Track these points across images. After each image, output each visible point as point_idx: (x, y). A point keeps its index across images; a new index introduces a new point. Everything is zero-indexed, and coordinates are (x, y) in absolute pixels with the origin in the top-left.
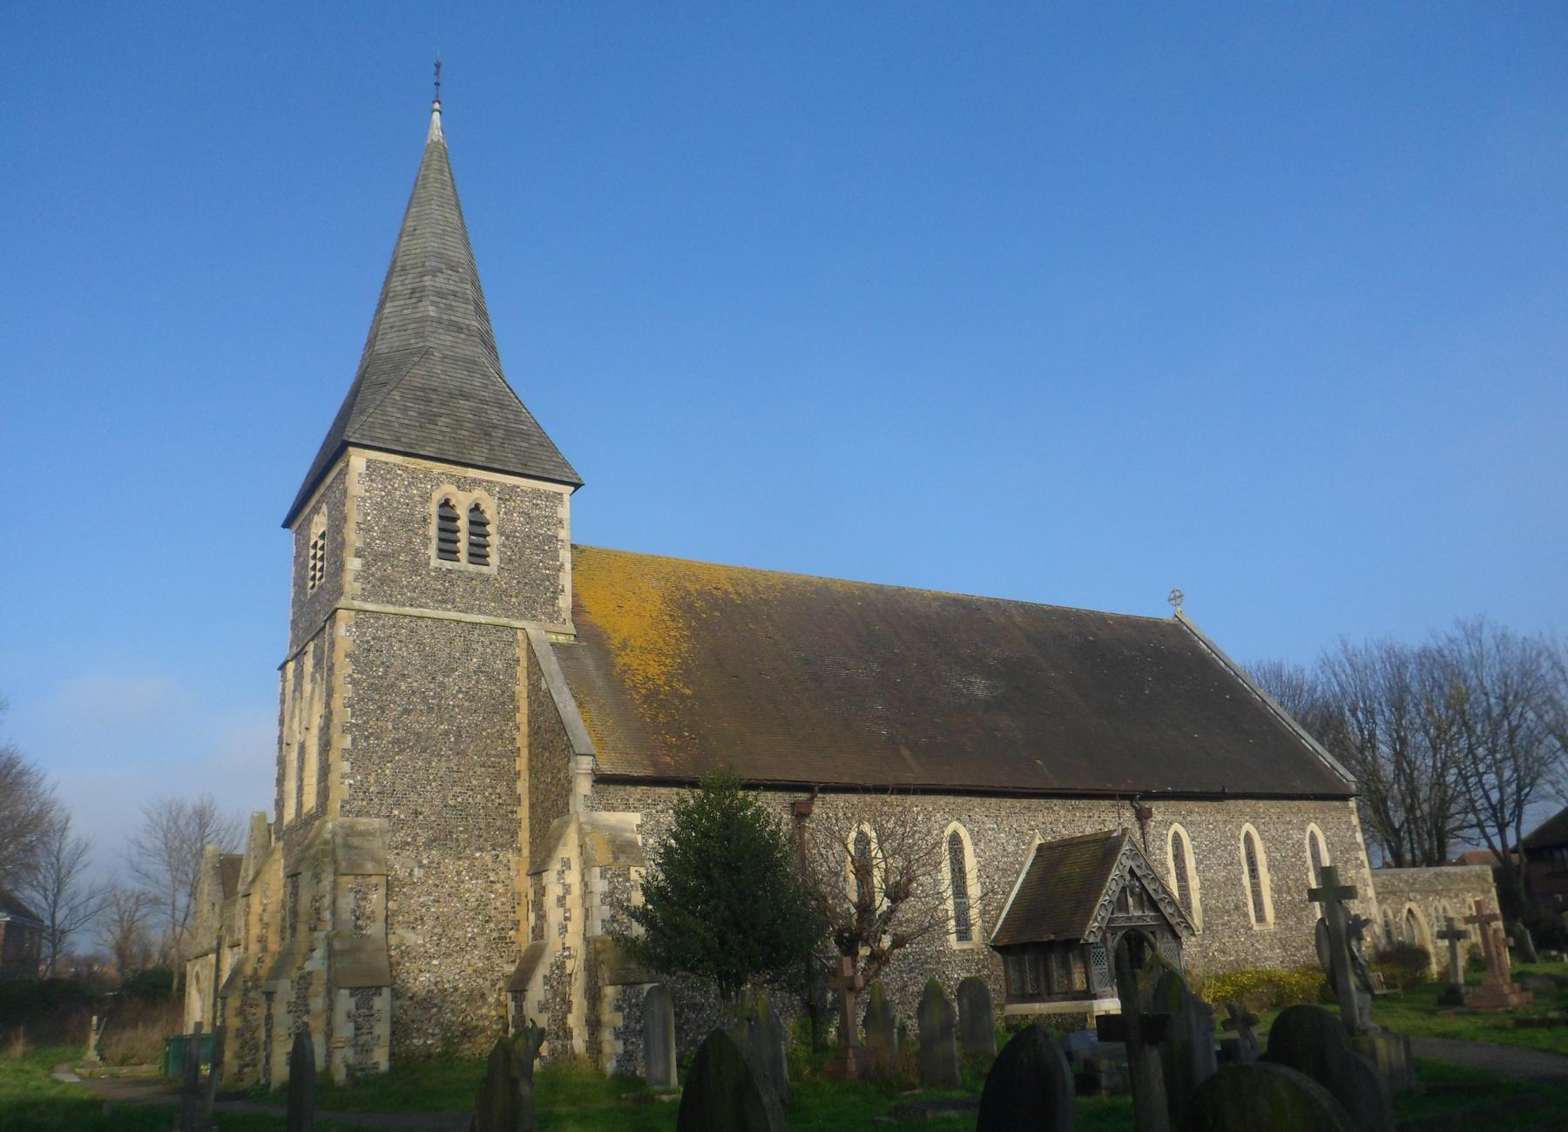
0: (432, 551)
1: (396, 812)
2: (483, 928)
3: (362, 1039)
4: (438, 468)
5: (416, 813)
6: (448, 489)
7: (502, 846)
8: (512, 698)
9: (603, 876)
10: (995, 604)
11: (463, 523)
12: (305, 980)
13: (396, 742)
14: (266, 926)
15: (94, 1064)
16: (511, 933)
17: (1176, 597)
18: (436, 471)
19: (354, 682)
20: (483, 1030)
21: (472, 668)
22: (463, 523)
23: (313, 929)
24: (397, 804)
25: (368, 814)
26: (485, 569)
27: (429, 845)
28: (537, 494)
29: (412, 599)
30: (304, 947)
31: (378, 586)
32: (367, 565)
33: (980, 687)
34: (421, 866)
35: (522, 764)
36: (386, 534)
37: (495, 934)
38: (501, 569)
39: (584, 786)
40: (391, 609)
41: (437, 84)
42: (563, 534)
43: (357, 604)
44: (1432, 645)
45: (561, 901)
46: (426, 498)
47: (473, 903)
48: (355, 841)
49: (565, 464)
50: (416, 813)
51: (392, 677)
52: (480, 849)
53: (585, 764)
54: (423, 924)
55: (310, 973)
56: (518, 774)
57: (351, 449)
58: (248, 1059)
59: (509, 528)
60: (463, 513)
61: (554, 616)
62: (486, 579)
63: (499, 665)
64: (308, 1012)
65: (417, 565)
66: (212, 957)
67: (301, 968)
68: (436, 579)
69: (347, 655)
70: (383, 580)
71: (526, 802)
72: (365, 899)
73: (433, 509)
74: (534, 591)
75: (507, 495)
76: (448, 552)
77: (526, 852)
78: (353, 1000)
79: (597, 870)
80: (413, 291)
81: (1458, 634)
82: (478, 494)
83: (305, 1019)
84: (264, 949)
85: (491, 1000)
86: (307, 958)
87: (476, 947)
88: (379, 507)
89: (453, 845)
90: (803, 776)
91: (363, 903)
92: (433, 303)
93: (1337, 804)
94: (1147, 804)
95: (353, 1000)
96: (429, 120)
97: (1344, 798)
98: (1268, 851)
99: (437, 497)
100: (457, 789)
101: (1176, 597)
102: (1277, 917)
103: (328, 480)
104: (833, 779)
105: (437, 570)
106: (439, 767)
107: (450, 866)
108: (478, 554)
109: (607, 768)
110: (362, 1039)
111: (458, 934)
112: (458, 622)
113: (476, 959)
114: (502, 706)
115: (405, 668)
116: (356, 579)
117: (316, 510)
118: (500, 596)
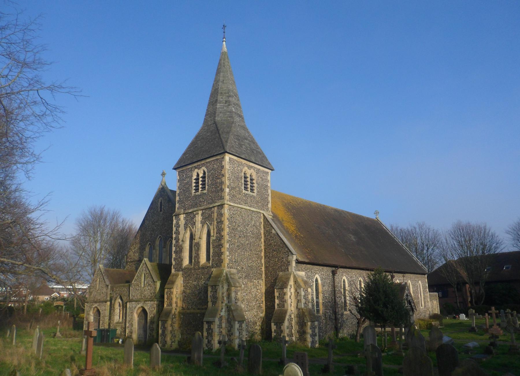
0: (243, 188)
4: (244, 161)
10: (343, 211)
11: (249, 179)
12: (221, 317)
13: (238, 246)
14: (177, 298)
15: (60, 337)
19: (229, 227)
22: (249, 179)
23: (222, 303)
24: (238, 265)
27: (245, 278)
30: (220, 308)
31: (233, 198)
32: (230, 191)
33: (353, 238)
35: (263, 254)
39: (294, 264)
40: (236, 205)
42: (269, 185)
44: (410, 229)
45: (290, 297)
49: (269, 163)
50: (242, 268)
52: (255, 279)
53: (295, 257)
59: (258, 182)
60: (248, 176)
61: (267, 210)
65: (240, 192)
66: (109, 303)
68: (244, 196)
73: (243, 175)
74: (263, 202)
76: (246, 188)
77: (264, 281)
81: (417, 226)
82: (252, 170)
84: (177, 306)
86: (221, 311)
92: (234, 107)
94: (394, 274)
96: (222, 45)
97: (425, 274)
99: (244, 171)
101: (377, 213)
103: (208, 160)
105: (244, 193)
106: (247, 254)
107: (249, 284)
108: (252, 190)
109: (300, 259)
110: (241, 336)
118: (257, 203)
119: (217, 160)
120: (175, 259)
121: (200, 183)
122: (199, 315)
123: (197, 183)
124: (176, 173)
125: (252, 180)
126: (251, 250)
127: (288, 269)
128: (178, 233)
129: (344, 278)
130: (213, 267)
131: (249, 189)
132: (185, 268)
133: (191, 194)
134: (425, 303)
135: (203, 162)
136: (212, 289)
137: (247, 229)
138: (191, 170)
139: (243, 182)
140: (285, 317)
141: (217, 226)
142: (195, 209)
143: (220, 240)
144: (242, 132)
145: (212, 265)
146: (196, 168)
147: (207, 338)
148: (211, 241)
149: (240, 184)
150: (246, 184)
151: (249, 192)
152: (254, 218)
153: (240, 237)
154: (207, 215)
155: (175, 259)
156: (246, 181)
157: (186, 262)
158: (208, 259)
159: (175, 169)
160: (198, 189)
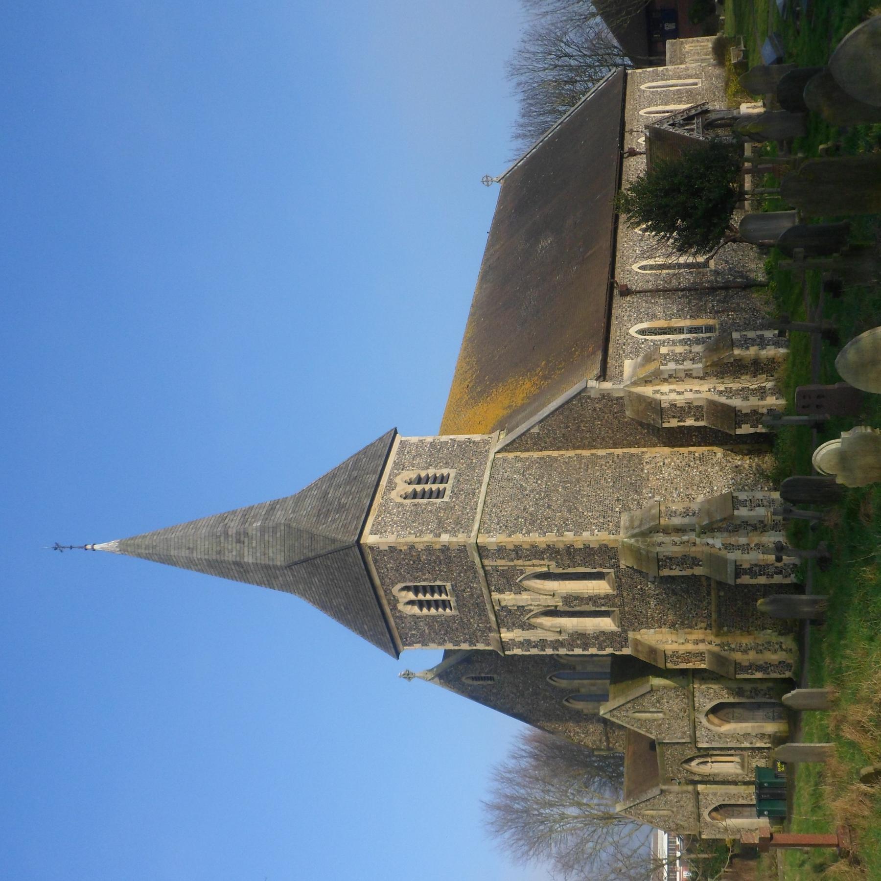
0: (439, 500)
2: (694, 468)
4: (378, 499)
5: (618, 500)
6: (393, 494)
8: (541, 458)
9: (666, 365)
13: (570, 511)
14: (687, 641)
16: (697, 455)
17: (487, 181)
18: (381, 501)
19: (528, 532)
20: (758, 465)
21: (521, 477)
22: (419, 488)
23: (694, 544)
24: (612, 509)
25: (619, 522)
26: (452, 476)
27: (639, 493)
28: (401, 452)
29: (471, 509)
31: (461, 524)
32: (446, 531)
33: (546, 242)
34: (654, 497)
35: (586, 453)
36: (426, 523)
37: (698, 462)
39: (607, 385)
41: (71, 548)
42: (429, 439)
43: (474, 533)
46: (401, 505)
47: (678, 473)
48: (636, 523)
49: (381, 439)
50: (618, 500)
52: (642, 470)
53: (592, 383)
54: (691, 495)
55: (723, 545)
56: (592, 455)
57: (362, 542)
58: (777, 646)
60: (410, 489)
61: (486, 443)
63: (519, 465)
64: (748, 545)
65: (448, 507)
66: (700, 787)
67: (720, 549)
69: (510, 536)
71: (612, 450)
72: (675, 512)
73: (408, 501)
74: (469, 454)
75: (400, 466)
76: (439, 494)
77: (645, 449)
78: (741, 508)
79: (662, 367)
80: (238, 541)
83: (752, 546)
84: (703, 641)
85: (739, 463)
86: (713, 546)
87: (706, 471)
89: (639, 482)
90: (604, 288)
91: (678, 513)
92: (251, 524)
93: (629, 77)
94: (626, 149)
95: (741, 508)
100: (602, 482)
104: (606, 275)
105: (451, 497)
106: (587, 490)
107: (653, 482)
108: (443, 479)
109: (596, 371)
110: (765, 503)
111: (697, 478)
112: (488, 484)
113: (713, 471)
114: (547, 464)
115: (519, 509)
116: (456, 536)
118: (470, 467)
119: (376, 561)
120: (601, 648)
121: (428, 597)
122: (722, 594)
125: (419, 481)
126: (578, 481)
128: (542, 644)
129: (635, 267)
130: (616, 566)
131: (441, 487)
133: (454, 617)
135: (381, 593)
136: (665, 566)
138: (401, 617)
139: (425, 501)
141: (527, 558)
142: (488, 607)
143: (558, 552)
145: (612, 567)
146: (394, 608)
148: (561, 571)
150: (431, 494)
151: (448, 486)
152: (506, 475)
153: (549, 507)
154: (503, 581)
155: (601, 648)
156: (423, 495)
157: (607, 624)
158: (599, 576)
159: (397, 654)
160: (444, 601)
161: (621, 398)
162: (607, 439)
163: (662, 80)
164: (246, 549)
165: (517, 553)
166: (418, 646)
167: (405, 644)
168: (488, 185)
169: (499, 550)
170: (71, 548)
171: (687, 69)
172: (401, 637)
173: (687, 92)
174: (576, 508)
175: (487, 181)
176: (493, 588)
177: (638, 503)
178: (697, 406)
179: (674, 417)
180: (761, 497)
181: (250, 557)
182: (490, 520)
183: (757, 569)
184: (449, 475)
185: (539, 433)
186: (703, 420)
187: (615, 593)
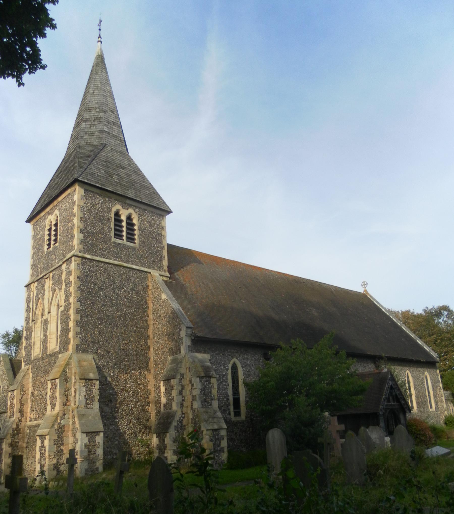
0: (112, 234)
1: (99, 351)
2: (136, 406)
3: (92, 456)
5: (108, 352)
7: (143, 368)
13: (99, 319)
24: (100, 348)
29: (104, 255)
38: (140, 246)
46: (110, 211)
50: (108, 352)
51: (97, 289)
52: (134, 369)
55: (64, 426)
60: (123, 218)
62: (134, 249)
63: (141, 287)
65: (106, 240)
68: (114, 247)
70: (92, 245)
73: (112, 215)
76: (118, 235)
78: (88, 438)
88: (90, 212)
95: (88, 438)
98: (414, 382)
99: (114, 210)
102: (417, 407)
108: (131, 238)
109: (199, 334)
110: (92, 456)
117: (50, 213)
123: (50, 235)
124: (29, 226)
126: (126, 326)
127: (180, 349)
131: (124, 238)
132: (37, 360)
133: (44, 252)
134: (436, 403)
137: (118, 295)
139: (112, 226)
140: (170, 423)
144: (117, 158)
145: (60, 349)
147: (39, 463)
149: (106, 228)
153: (103, 305)
161: (180, 352)
162: (158, 346)
163: (433, 386)
164: (90, 123)
165: (68, 284)
166: (32, 233)
167: (34, 225)
168: (367, 284)
169: (70, 271)
170: (100, 30)
171: (442, 402)
172: (37, 221)
173: (425, 402)
174: (102, 323)
175: (364, 284)
176: (54, 273)
177: (105, 366)
178: (172, 405)
179: (166, 389)
180: (97, 453)
181: (84, 126)
182: (93, 266)
183: (43, 451)
184: (135, 243)
185: (161, 299)
186: (164, 410)
187: (48, 353)
